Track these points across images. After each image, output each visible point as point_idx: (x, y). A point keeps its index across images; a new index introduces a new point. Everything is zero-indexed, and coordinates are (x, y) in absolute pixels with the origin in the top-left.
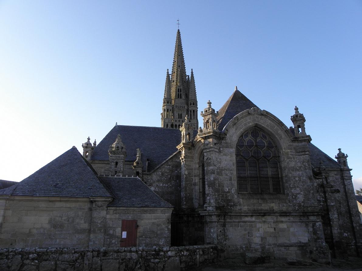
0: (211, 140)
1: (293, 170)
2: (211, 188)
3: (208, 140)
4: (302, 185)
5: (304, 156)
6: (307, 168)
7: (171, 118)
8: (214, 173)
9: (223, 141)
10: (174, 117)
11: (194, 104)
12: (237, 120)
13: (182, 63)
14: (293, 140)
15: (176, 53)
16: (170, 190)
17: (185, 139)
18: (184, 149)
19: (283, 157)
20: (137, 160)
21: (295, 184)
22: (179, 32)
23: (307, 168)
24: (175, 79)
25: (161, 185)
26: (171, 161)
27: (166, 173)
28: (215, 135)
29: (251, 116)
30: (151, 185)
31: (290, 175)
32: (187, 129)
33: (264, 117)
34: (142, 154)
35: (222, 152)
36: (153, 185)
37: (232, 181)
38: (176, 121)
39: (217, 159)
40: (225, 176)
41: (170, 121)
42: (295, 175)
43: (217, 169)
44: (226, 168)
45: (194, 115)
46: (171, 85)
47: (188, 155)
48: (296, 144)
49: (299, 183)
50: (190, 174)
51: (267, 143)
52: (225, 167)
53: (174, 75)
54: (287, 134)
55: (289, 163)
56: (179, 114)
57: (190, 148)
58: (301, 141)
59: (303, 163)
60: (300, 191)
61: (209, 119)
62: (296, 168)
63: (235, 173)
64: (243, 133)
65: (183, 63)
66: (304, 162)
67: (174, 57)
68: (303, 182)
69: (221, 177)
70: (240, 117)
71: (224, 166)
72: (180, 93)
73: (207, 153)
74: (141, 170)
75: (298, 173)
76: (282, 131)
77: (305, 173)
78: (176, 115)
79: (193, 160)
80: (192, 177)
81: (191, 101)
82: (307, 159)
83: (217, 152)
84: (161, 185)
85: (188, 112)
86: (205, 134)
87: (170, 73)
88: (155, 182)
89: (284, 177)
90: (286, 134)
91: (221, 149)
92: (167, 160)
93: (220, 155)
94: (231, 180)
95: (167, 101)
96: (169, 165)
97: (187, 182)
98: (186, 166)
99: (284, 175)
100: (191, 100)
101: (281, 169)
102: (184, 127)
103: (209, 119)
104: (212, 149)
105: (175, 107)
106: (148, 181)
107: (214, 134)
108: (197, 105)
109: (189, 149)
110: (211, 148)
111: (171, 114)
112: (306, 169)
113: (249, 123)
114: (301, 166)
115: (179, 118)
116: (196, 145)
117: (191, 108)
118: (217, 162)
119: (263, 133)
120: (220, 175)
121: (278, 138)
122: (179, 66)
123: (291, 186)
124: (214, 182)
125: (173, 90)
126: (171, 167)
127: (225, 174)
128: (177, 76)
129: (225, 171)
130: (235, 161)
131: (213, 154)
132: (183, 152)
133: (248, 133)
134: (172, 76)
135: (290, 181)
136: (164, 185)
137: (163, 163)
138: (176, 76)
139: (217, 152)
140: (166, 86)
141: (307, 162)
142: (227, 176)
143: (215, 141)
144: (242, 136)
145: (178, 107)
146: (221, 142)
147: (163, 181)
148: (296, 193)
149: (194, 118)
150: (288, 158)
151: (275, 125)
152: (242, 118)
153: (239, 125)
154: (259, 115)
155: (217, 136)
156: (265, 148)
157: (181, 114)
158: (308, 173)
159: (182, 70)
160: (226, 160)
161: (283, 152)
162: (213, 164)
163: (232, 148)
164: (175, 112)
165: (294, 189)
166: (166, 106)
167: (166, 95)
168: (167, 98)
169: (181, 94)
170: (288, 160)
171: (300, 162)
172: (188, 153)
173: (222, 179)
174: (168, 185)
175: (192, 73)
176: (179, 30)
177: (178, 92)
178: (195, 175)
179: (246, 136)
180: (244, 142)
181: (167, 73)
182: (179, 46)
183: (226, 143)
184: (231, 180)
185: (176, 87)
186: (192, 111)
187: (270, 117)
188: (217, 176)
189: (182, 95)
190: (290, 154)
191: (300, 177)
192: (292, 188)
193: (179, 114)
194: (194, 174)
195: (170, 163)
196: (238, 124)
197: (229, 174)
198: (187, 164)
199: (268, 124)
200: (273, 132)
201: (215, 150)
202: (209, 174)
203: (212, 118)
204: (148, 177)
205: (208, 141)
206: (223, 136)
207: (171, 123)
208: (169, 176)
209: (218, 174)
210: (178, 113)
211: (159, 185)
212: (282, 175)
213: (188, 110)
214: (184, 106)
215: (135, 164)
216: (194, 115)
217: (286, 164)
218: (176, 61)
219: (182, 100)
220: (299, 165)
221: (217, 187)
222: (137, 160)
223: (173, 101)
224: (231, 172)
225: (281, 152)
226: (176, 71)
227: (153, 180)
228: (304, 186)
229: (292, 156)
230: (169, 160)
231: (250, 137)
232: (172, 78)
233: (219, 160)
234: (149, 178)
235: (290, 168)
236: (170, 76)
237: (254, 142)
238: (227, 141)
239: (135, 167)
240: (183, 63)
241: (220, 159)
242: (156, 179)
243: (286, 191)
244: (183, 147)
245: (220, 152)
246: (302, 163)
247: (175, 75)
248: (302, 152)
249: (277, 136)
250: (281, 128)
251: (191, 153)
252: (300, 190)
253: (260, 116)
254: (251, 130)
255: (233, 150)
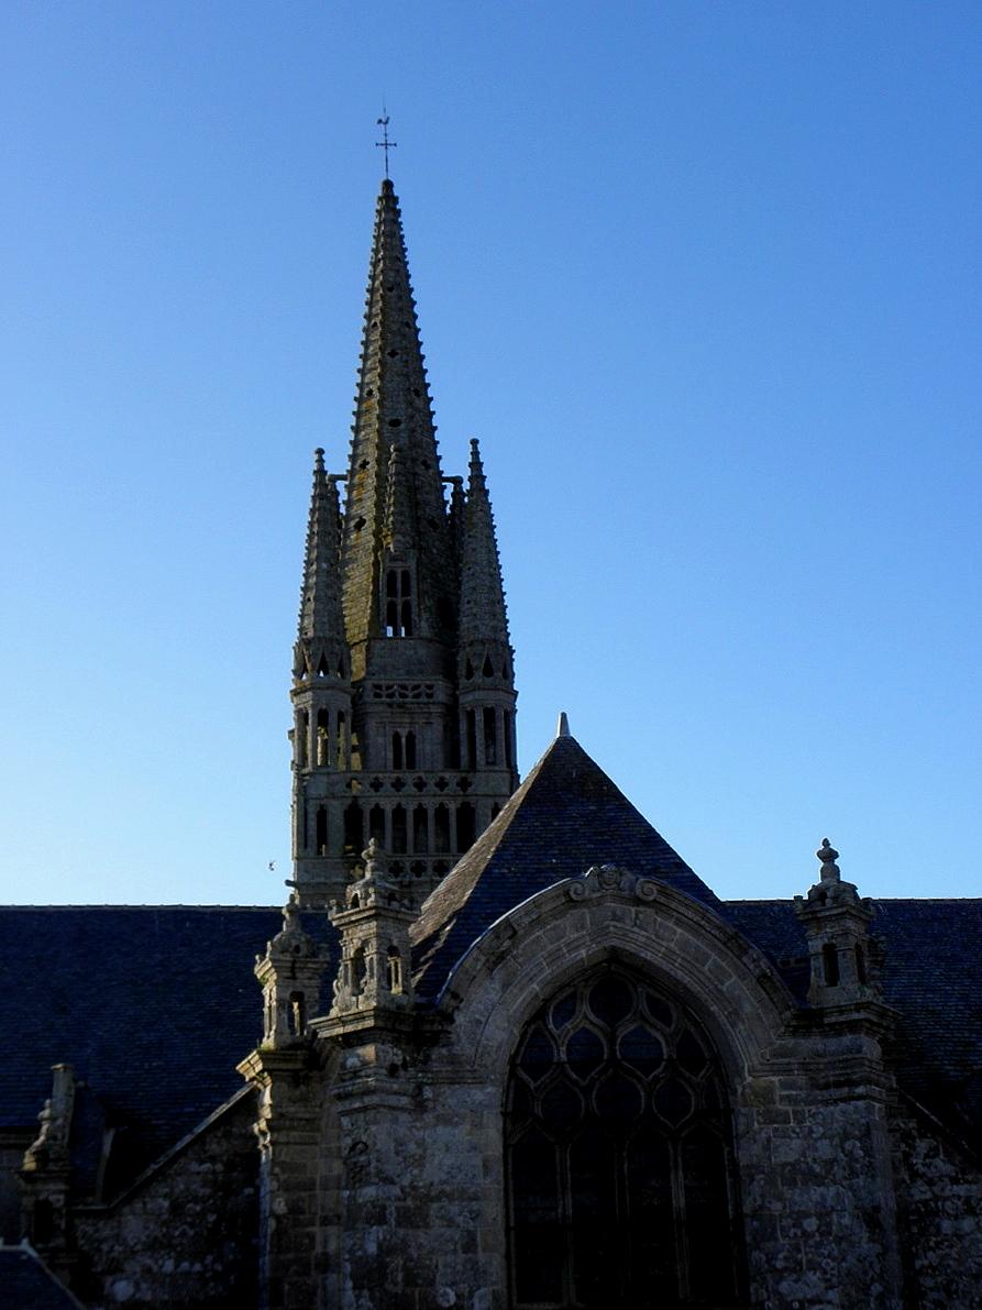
0: (369, 1051)
1: (792, 1183)
2: (366, 1292)
3: (361, 1051)
4: (836, 1253)
5: (850, 1107)
6: (858, 1166)
7: (349, 770)
8: (381, 1219)
9: (435, 1053)
10: (364, 761)
11: (488, 672)
12: (510, 938)
13: (411, 404)
14: (794, 1023)
15: (376, 336)
16: (213, 1293)
17: (274, 1027)
18: (268, 1080)
19: (745, 1115)
20: (42, 1138)
21: (799, 1251)
22: (389, 199)
23: (858, 1166)
24: (367, 510)
25: (169, 1266)
26: (219, 1134)
27: (195, 1200)
28: (389, 1025)
29: (586, 910)
30: (115, 1269)
31: (777, 1206)
32: (288, 973)
33: (649, 910)
34: (78, 1090)
35: (430, 1104)
36: (123, 1271)
37: (475, 1252)
38: (377, 785)
39: (400, 1143)
40: (443, 1230)
41: (341, 787)
42: (803, 1208)
43: (398, 1199)
44: (448, 1188)
45: (491, 736)
46: (345, 549)
47: (292, 1109)
48: (813, 1043)
49: (818, 1245)
50: (303, 1213)
51: (668, 1045)
52: (444, 1182)
53: (361, 485)
54: (767, 993)
55: (776, 1142)
56: (397, 737)
57: (302, 1074)
58: (838, 1030)
59: (842, 1142)
60: (823, 1285)
61: (365, 943)
62: (811, 1170)
63: (494, 1210)
64: (547, 1001)
65: (419, 403)
66: (846, 1136)
67: (361, 350)
68: (839, 1240)
69: (421, 1233)
70: (526, 920)
71: (436, 1180)
72: (399, 601)
73: (354, 1117)
74: (60, 1192)
75: (816, 1193)
76: (742, 977)
77: (850, 1194)
78: (380, 742)
79: (317, 1135)
80: (313, 1225)
81: (468, 649)
82: (863, 1121)
83: (402, 1109)
84: (169, 1266)
85: (456, 721)
86: (344, 1023)
87: (338, 464)
88: (134, 1253)
89: (747, 1215)
90: (764, 995)
91: (428, 1093)
92: (200, 1129)
93: (418, 1124)
94: (470, 1245)
95: (320, 653)
96: (213, 1159)
97: (282, 1257)
98: (277, 1170)
99: (747, 1209)
100: (471, 644)
101: (735, 1173)
102: (270, 965)
103: (365, 943)
104: (375, 1099)
105: (369, 697)
106: (100, 1250)
107: (381, 1024)
108: (508, 675)
109: (296, 1079)
110: (369, 1092)
111: (346, 738)
112: (854, 1174)
113: (573, 947)
114: (835, 1160)
115: (397, 765)
116: (328, 1058)
117: (470, 697)
118: (401, 1159)
119: (651, 991)
120: (419, 1227)
121: (722, 1019)
122: (395, 423)
123: (779, 1264)
124: (383, 1267)
125: (359, 580)
126: (219, 1167)
127: (442, 1218)
128: (380, 489)
129: (445, 1202)
130: (495, 1148)
131: (376, 1122)
132: (267, 1099)
133: (573, 996)
134: (350, 489)
135: (776, 1240)
136: (185, 1265)
137: (179, 1146)
138: (377, 489)
139: (402, 1109)
140: (308, 563)
141: (859, 1139)
142: (449, 1226)
143: (396, 1055)
144: (539, 1015)
145: (391, 696)
146: (428, 1058)
147: (181, 1244)
148: (800, 1296)
149: (494, 763)
150: (771, 1117)
151: (707, 950)
152: (538, 922)
153: (520, 960)
154: (622, 900)
155: (400, 1032)
156: (660, 1069)
157: (411, 738)
158: (863, 1194)
159: (414, 445)
160: (457, 1145)
161: (744, 1088)
162: (379, 1172)
163: (481, 1082)
164: (372, 725)
165: (795, 1276)
166: (309, 694)
167: (308, 622)
168: (317, 639)
169: (407, 606)
170: (769, 1130)
171: (831, 1138)
172: (290, 1099)
173: (425, 1243)
174: (205, 1266)
175: (476, 465)
176: (388, 185)
177: (392, 591)
178: (325, 1218)
179: (565, 1011)
180: (552, 1043)
181: (317, 461)
182: (390, 290)
183: (453, 1060)
184: (470, 1245)
185: (376, 564)
186: (479, 717)
187: (682, 910)
188: (401, 1232)
189: (415, 610)
190: (782, 1098)
191: (828, 1214)
192: (780, 1275)
193: (397, 737)
194: (323, 1208)
195: (214, 1148)
196: (515, 957)
197: (460, 1219)
198: (284, 1162)
199: (672, 945)
200: (696, 988)
201: (392, 1100)
202: (359, 1226)
203: (378, 936)
204: (97, 1231)
205: (358, 1056)
206: (437, 1027)
207: (349, 801)
208: (212, 1218)
209: (407, 1219)
210: (390, 731)
211: (155, 1268)
212: (738, 1205)
213: (451, 711)
214: (430, 687)
215: (29, 1163)
216: (491, 736)
217: (756, 1149)
218: (376, 393)
219: (411, 646)
220: (825, 1149)
221: (399, 1289)
222: (42, 1138)
223: (358, 658)
224: (475, 1205)
225: (736, 1091)
226: (371, 454)
227: (125, 1239)
228: (844, 1259)
229: (790, 1109)
230: (206, 1129)
231: (585, 1017)
232: (348, 503)
233: (412, 1147)
234: (107, 1232)
235: (779, 1169)
236: (341, 485)
237: (604, 1043)
238: (457, 1049)
239: (29, 1177)
240: (419, 403)
241: (421, 1144)
242: (144, 1239)
243: (756, 1290)
244: (262, 1071)
245: (420, 1106)
246: (836, 1141)
247: (371, 481)
248: (838, 1085)
249: (714, 1008)
250: (739, 963)
251: (304, 1100)
252: (827, 1281)
253: (633, 909)
254: (586, 981)
255: (487, 1095)
